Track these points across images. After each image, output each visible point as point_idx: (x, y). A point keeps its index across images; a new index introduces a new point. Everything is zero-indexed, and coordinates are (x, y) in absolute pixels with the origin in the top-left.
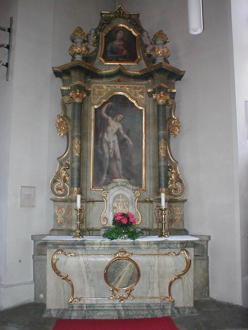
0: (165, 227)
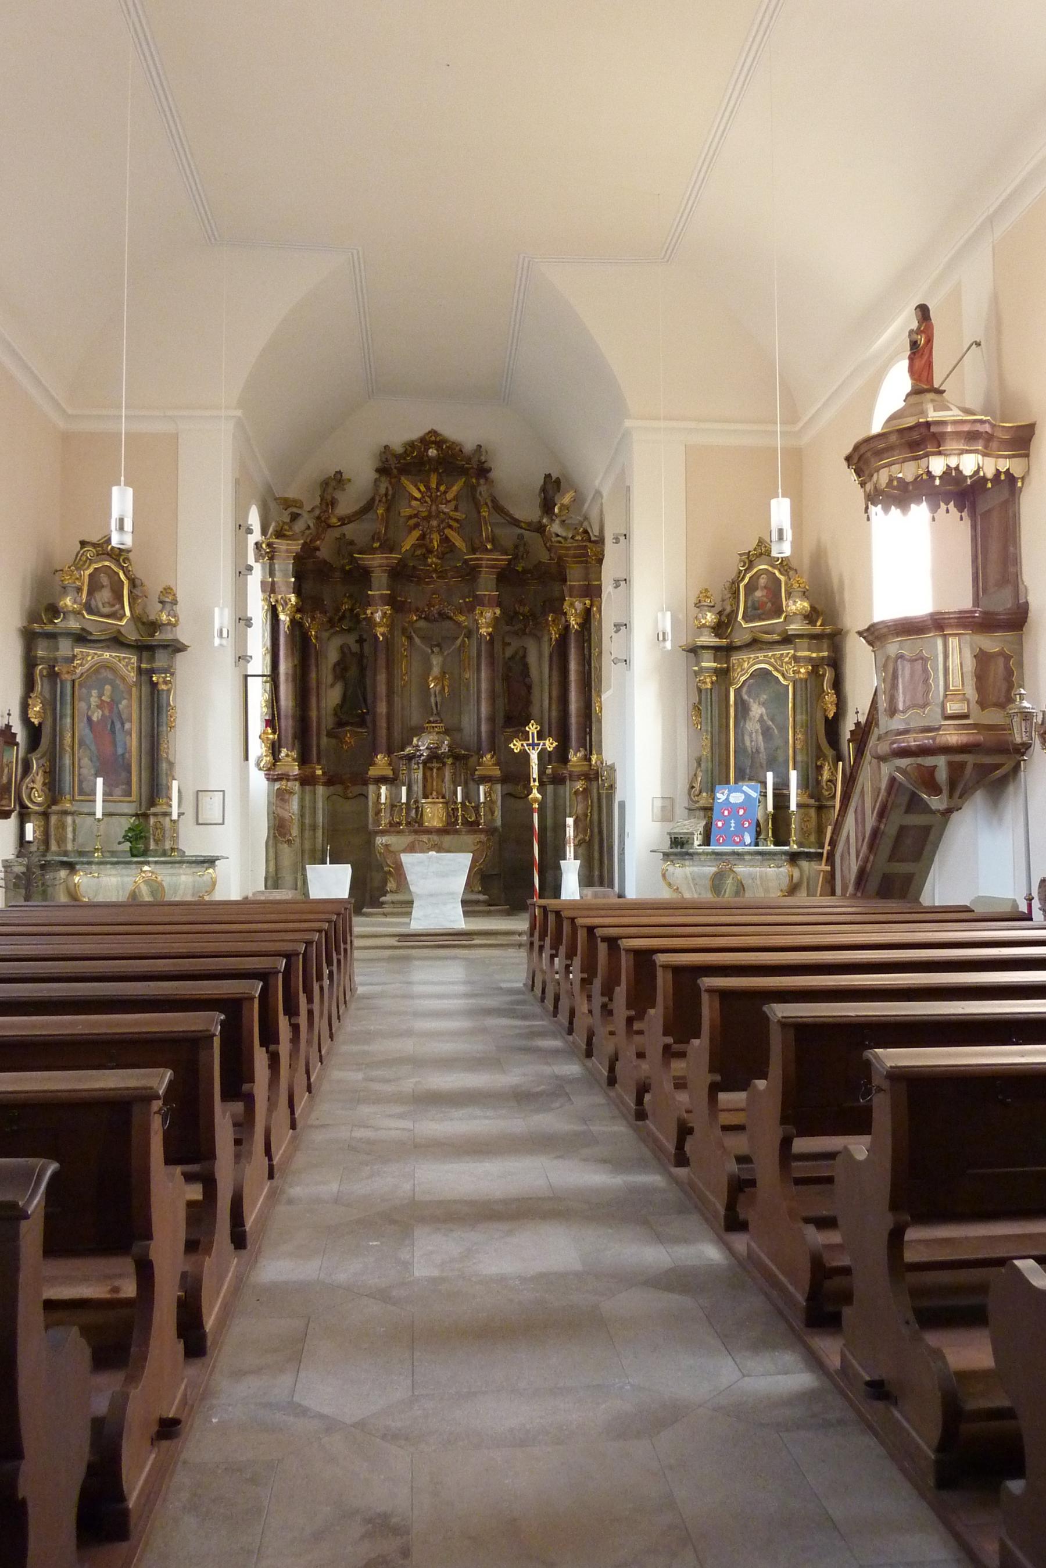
0: (176, 919)
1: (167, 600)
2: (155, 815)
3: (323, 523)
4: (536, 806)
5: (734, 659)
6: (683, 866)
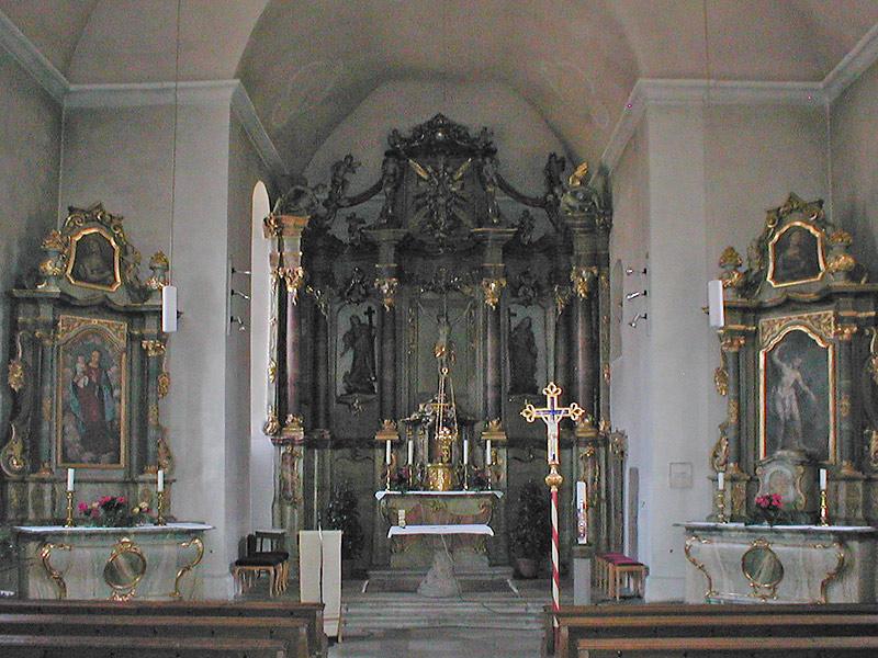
1: (157, 265)
2: (144, 482)
3: (333, 204)
4: (554, 489)
5: (763, 322)
6: (711, 542)
